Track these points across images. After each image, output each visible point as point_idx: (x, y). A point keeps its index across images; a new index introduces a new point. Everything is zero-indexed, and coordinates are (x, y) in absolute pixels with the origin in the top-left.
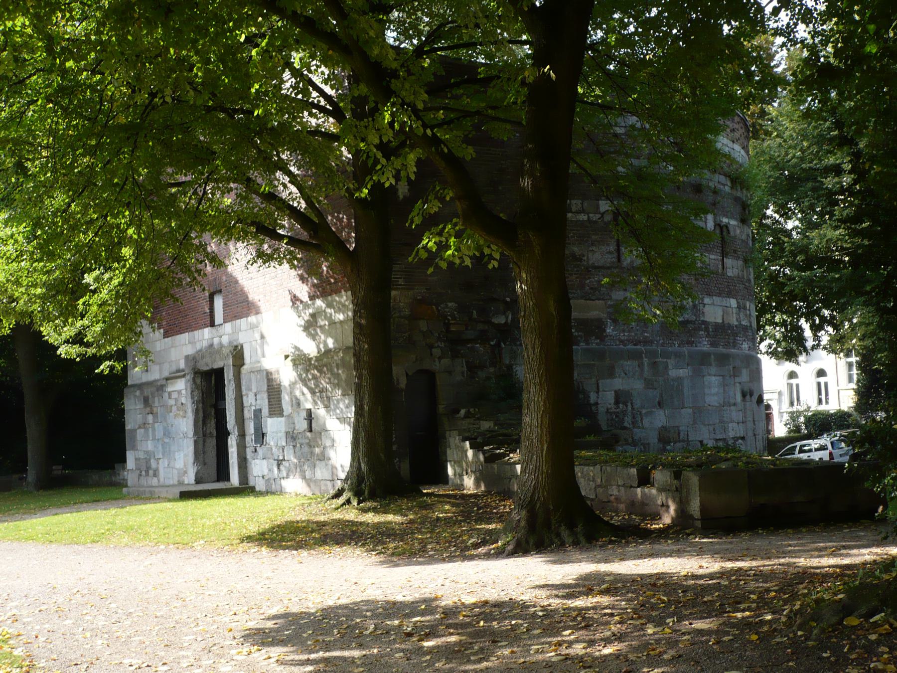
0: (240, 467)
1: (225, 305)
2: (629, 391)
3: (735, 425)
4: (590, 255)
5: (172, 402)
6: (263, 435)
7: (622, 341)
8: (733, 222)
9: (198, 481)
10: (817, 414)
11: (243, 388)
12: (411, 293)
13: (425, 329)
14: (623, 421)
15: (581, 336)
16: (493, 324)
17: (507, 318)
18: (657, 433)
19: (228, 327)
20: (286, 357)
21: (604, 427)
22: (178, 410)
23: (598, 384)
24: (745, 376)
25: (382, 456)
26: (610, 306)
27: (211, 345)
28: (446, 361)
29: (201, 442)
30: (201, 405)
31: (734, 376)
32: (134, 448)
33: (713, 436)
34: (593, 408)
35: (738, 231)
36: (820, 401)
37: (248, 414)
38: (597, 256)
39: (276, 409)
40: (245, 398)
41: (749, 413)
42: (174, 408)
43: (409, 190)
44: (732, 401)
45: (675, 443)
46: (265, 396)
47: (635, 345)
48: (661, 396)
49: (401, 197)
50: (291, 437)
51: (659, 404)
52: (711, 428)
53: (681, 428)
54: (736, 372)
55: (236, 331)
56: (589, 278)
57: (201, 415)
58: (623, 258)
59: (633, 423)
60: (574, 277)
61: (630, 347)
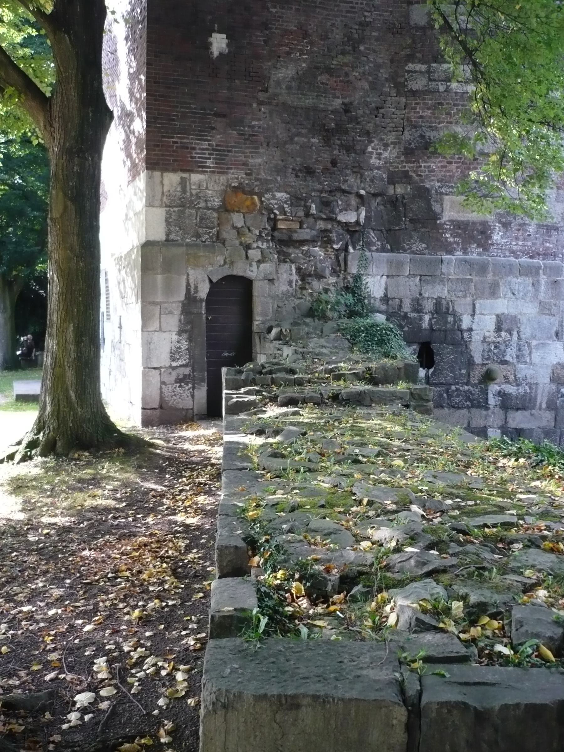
2: (516, 317)
12: (223, 178)
13: (240, 224)
15: (458, 244)
16: (339, 223)
17: (359, 215)
18: (550, 371)
20: (113, 255)
21: (478, 359)
23: (474, 305)
25: (72, 394)
34: (466, 335)
43: (228, 45)
47: (531, 257)
49: (216, 53)
51: (557, 334)
59: (518, 357)
60: (454, 166)
61: (524, 260)
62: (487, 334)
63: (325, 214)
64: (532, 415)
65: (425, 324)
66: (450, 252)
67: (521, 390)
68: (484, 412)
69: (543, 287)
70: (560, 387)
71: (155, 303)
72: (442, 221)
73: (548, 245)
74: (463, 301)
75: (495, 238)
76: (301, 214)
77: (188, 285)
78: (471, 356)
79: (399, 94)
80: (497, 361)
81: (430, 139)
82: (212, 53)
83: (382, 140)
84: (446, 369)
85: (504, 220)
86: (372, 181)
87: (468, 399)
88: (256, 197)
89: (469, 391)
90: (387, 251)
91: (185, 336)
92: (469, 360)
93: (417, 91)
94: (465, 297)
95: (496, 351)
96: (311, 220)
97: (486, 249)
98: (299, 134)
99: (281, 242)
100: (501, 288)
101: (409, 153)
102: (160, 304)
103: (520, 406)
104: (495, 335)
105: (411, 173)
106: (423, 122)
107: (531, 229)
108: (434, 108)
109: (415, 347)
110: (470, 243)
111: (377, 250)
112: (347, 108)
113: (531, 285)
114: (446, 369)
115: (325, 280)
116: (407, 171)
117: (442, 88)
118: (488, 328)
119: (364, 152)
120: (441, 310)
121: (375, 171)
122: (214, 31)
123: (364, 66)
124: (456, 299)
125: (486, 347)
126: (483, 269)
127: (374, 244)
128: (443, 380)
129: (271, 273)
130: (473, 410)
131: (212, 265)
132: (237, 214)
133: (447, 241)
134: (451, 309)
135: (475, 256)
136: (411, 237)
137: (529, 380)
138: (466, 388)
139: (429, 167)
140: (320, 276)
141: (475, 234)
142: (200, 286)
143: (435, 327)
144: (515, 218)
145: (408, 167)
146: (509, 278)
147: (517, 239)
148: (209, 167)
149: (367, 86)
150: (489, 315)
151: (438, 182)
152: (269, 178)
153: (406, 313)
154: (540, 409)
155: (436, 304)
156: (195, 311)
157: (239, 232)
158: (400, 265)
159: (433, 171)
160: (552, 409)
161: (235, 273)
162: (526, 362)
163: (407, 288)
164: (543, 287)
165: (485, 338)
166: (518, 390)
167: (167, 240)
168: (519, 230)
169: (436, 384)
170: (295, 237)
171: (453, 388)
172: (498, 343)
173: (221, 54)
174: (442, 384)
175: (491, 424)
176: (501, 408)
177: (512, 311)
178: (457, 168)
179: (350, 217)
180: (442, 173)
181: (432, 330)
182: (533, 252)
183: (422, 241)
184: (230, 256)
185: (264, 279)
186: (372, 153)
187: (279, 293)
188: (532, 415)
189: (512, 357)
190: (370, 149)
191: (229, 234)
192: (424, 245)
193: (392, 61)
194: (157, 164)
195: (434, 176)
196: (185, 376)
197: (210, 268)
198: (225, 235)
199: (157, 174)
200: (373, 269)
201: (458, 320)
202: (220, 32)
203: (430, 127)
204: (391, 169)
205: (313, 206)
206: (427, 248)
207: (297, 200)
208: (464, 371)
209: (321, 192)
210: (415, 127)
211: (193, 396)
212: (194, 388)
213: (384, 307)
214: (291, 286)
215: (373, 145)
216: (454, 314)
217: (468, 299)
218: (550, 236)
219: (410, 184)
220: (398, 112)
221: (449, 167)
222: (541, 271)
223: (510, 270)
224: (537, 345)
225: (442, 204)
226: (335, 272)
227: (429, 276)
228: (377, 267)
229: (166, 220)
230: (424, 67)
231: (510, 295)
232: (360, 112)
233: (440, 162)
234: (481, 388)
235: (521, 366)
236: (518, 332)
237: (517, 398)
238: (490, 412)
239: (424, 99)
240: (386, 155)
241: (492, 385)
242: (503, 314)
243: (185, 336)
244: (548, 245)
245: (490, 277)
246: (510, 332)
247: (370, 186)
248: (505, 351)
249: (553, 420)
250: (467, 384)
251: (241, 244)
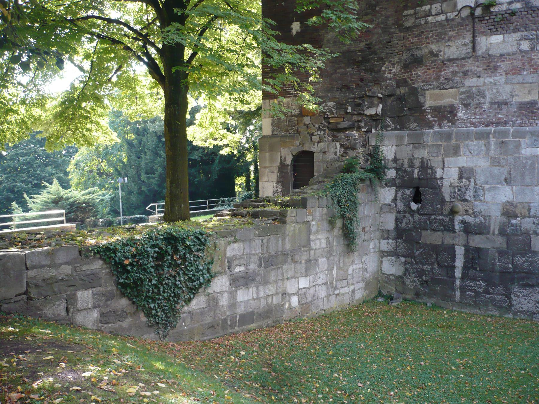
2: (472, 169)
4: (446, 50)
7: (473, 124)
15: (435, 121)
16: (367, 115)
18: (500, 207)
23: (443, 162)
26: (462, 93)
34: (439, 182)
38: (453, 49)
43: (301, 27)
45: (524, 217)
47: (487, 126)
51: (506, 180)
56: (445, 70)
58: (477, 48)
59: (474, 196)
61: (482, 128)
62: (453, 181)
63: (357, 111)
64: (487, 238)
65: (416, 176)
66: (431, 127)
67: (477, 220)
68: (453, 235)
69: (493, 147)
70: (510, 219)
71: (266, 168)
72: (425, 107)
73: (499, 116)
74: (436, 159)
75: (459, 115)
76: (342, 113)
77: (281, 157)
78: (443, 196)
79: (400, 31)
80: (460, 200)
81: (417, 56)
82: (292, 33)
83: (390, 61)
84: (428, 205)
85: (465, 102)
86: (386, 87)
87: (442, 225)
89: (442, 220)
90: (398, 130)
91: (280, 184)
92: (442, 199)
93: (409, 27)
94: (438, 156)
95: (459, 193)
96: (349, 116)
97: (453, 123)
98: (340, 68)
99: (332, 130)
100: (461, 149)
101: (406, 67)
102: (267, 167)
103: (477, 231)
104: (458, 181)
105: (408, 80)
106: (413, 46)
107: (485, 106)
108: (419, 35)
109: (411, 190)
110: (443, 120)
111: (392, 130)
112: (369, 46)
113: (483, 146)
114: (428, 205)
115: (356, 150)
116: (406, 78)
117: (423, 22)
118: (454, 177)
119: (380, 71)
120: (424, 166)
121: (388, 81)
122: (294, 21)
123: (378, 19)
124: (432, 158)
125: (452, 190)
126: (448, 136)
127: (389, 126)
128: (426, 212)
129: (324, 148)
130: (445, 233)
131: (293, 146)
132: (306, 117)
133: (429, 120)
134: (429, 165)
135: (446, 129)
136: (410, 120)
137: (483, 213)
138: (440, 217)
139: (417, 74)
140: (354, 149)
141: (447, 114)
144: (473, 100)
145: (406, 75)
146: (467, 142)
147: (475, 114)
148: (292, 94)
149: (380, 31)
150: (454, 168)
151: (422, 82)
152: (323, 95)
154: (494, 234)
156: (285, 171)
157: (308, 127)
158: (401, 138)
159: (419, 76)
160: (504, 235)
161: (304, 149)
162: (481, 201)
163: (406, 153)
164: (493, 147)
165: (451, 184)
166: (475, 220)
167: (272, 135)
168: (476, 108)
169: (422, 214)
170: (340, 126)
171: (433, 217)
172: (461, 187)
173: (297, 33)
174: (426, 214)
175: (457, 243)
176: (464, 232)
177: (470, 165)
178: (434, 71)
179: (371, 112)
180: (425, 77)
181: (419, 178)
182: (488, 122)
183: (415, 122)
184: (302, 141)
185: (321, 152)
186: (385, 70)
187: (329, 159)
188: (487, 238)
189: (471, 197)
190: (383, 68)
191: (302, 129)
192: (416, 124)
193: (396, 12)
194: (267, 96)
195: (419, 79)
197: (292, 148)
198: (300, 129)
199: (267, 101)
200: (386, 142)
201: (434, 172)
202: (296, 21)
203: (417, 48)
204: (398, 78)
205: (349, 108)
206: (418, 126)
207: (340, 106)
208: (439, 206)
209: (354, 98)
210: (409, 50)
213: (394, 165)
214: (336, 155)
215: (385, 65)
216: (431, 168)
217: (440, 158)
218: (501, 109)
219: (407, 86)
220: (400, 43)
221: (429, 72)
222: (491, 136)
223: (468, 136)
224: (490, 188)
225: (425, 97)
226: (364, 146)
227: (417, 144)
228: (389, 140)
229: (272, 124)
231: (468, 153)
232: (377, 47)
233: (423, 69)
234: (450, 218)
235: (477, 203)
236: (475, 180)
237: (474, 225)
238: (456, 235)
239: (413, 31)
240: (394, 70)
241: (457, 216)
242: (463, 167)
243: (280, 184)
244: (499, 116)
245: (453, 142)
246: (468, 179)
247: (385, 91)
248: (465, 193)
249: (505, 243)
250: (441, 214)
251: (308, 133)
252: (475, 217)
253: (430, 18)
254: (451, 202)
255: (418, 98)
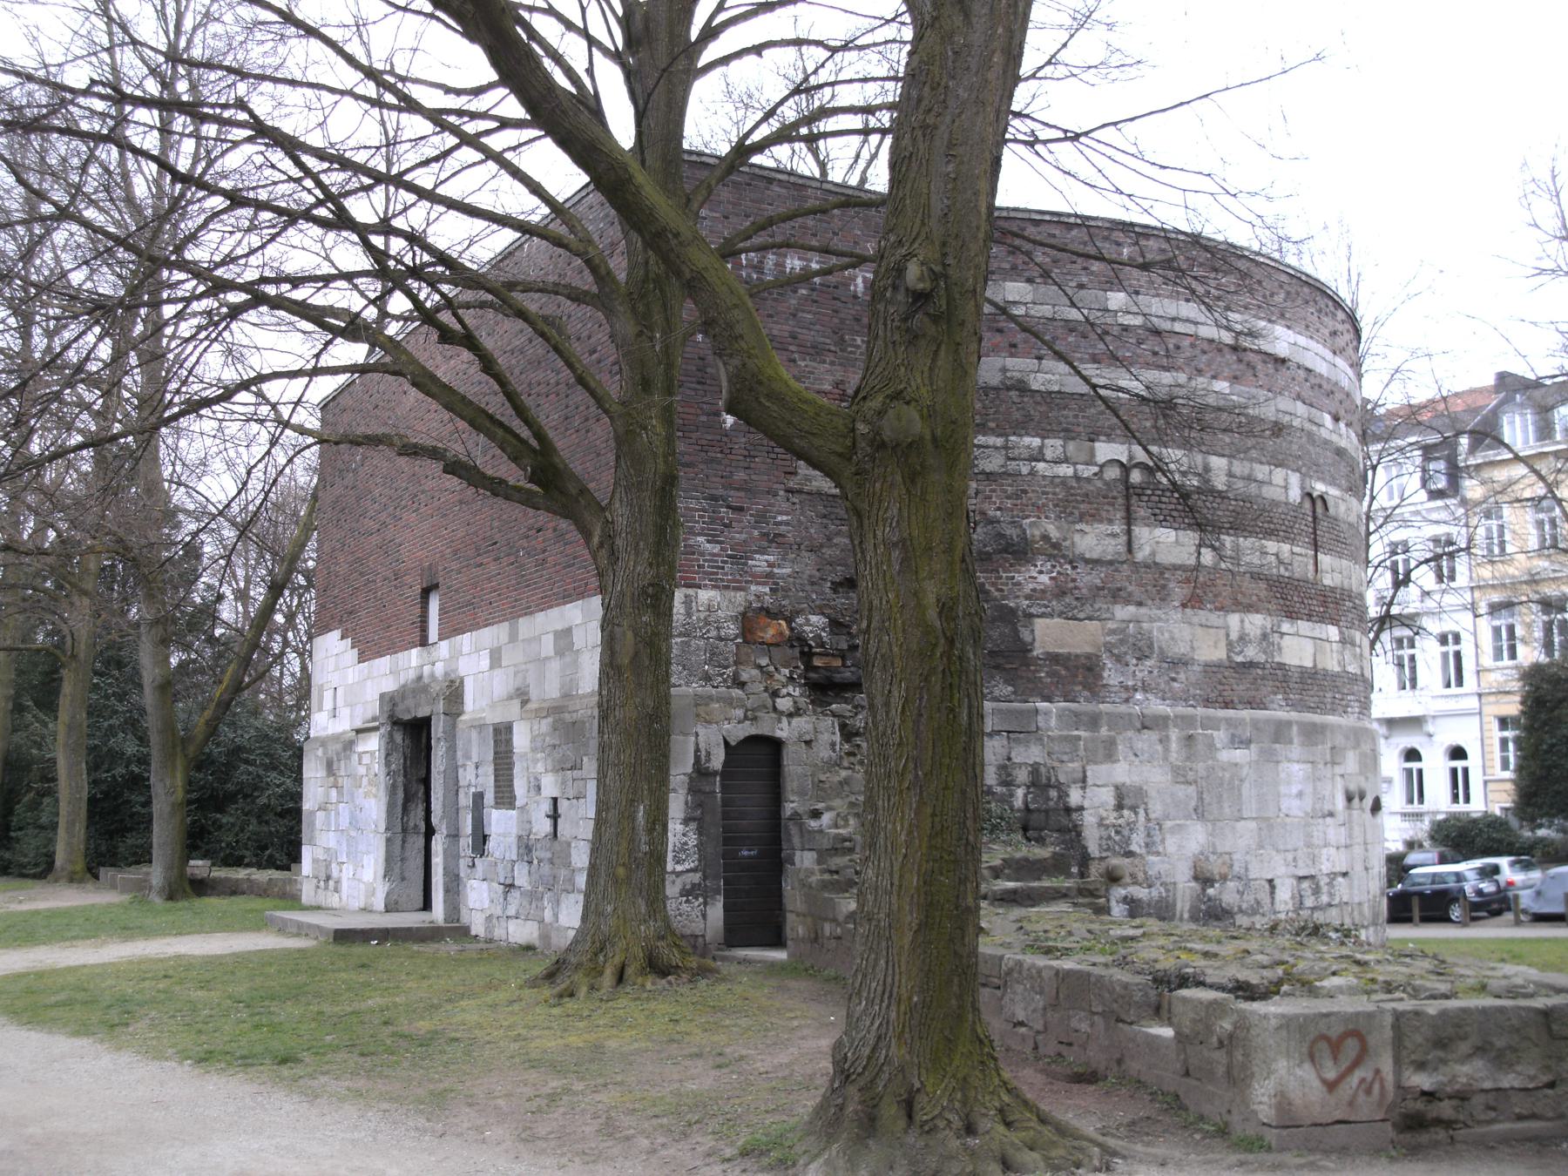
0: (447, 891)
1: (443, 611)
3: (1332, 851)
4: (1077, 538)
5: (362, 770)
6: (485, 838)
8: (1333, 492)
9: (389, 908)
10: (1454, 817)
11: (459, 754)
14: (1128, 841)
19: (444, 644)
21: (1093, 849)
22: (370, 783)
24: (1351, 763)
26: (1113, 632)
27: (420, 678)
28: (802, 724)
29: (398, 842)
30: (400, 779)
31: (1334, 763)
32: (312, 843)
33: (1292, 871)
35: (1342, 508)
36: (1455, 798)
37: (465, 800)
39: (505, 797)
40: (461, 771)
41: (1357, 831)
42: (365, 780)
44: (1327, 807)
46: (491, 769)
48: (1201, 799)
50: (526, 847)
52: (1290, 856)
53: (1235, 857)
54: (1335, 758)
55: (456, 654)
57: (400, 795)
58: (1135, 546)
59: (1147, 845)
62: (1105, 814)
67: (1155, 893)
77: (697, 750)
88: (783, 623)
91: (693, 825)
104: (1115, 814)
105: (987, 587)
117: (1025, 470)
125: (1105, 834)
142: (714, 751)
143: (1032, 806)
153: (990, 787)
154: (1181, 919)
155: (1031, 773)
170: (838, 677)
181: (1027, 809)
183: (1007, 682)
192: (1010, 689)
196: (694, 885)
206: (1014, 693)
211: (704, 916)
212: (705, 904)
216: (1059, 786)
230: (999, 441)
236: (1146, 811)
243: (693, 825)
246: (1134, 809)
252: (1150, 886)
253: (1041, 466)
254: (1102, 859)
255: (1016, 632)
